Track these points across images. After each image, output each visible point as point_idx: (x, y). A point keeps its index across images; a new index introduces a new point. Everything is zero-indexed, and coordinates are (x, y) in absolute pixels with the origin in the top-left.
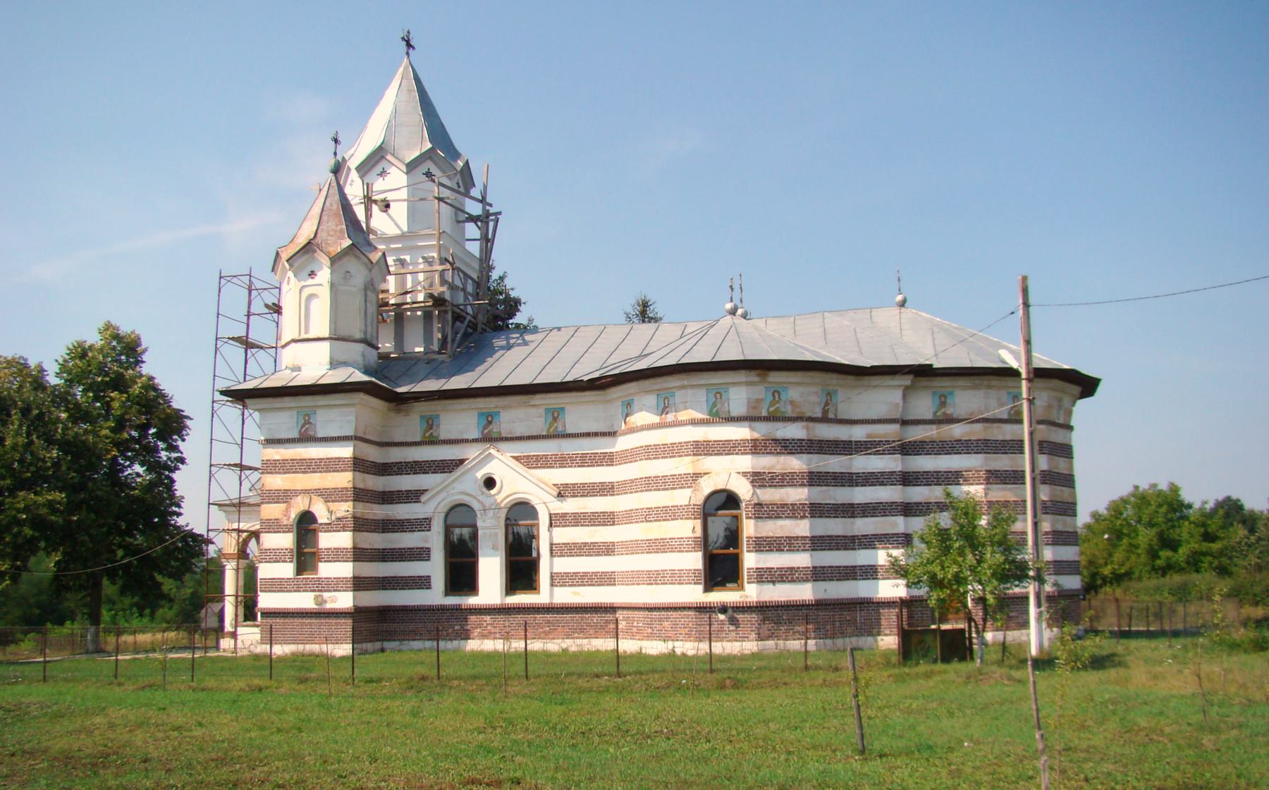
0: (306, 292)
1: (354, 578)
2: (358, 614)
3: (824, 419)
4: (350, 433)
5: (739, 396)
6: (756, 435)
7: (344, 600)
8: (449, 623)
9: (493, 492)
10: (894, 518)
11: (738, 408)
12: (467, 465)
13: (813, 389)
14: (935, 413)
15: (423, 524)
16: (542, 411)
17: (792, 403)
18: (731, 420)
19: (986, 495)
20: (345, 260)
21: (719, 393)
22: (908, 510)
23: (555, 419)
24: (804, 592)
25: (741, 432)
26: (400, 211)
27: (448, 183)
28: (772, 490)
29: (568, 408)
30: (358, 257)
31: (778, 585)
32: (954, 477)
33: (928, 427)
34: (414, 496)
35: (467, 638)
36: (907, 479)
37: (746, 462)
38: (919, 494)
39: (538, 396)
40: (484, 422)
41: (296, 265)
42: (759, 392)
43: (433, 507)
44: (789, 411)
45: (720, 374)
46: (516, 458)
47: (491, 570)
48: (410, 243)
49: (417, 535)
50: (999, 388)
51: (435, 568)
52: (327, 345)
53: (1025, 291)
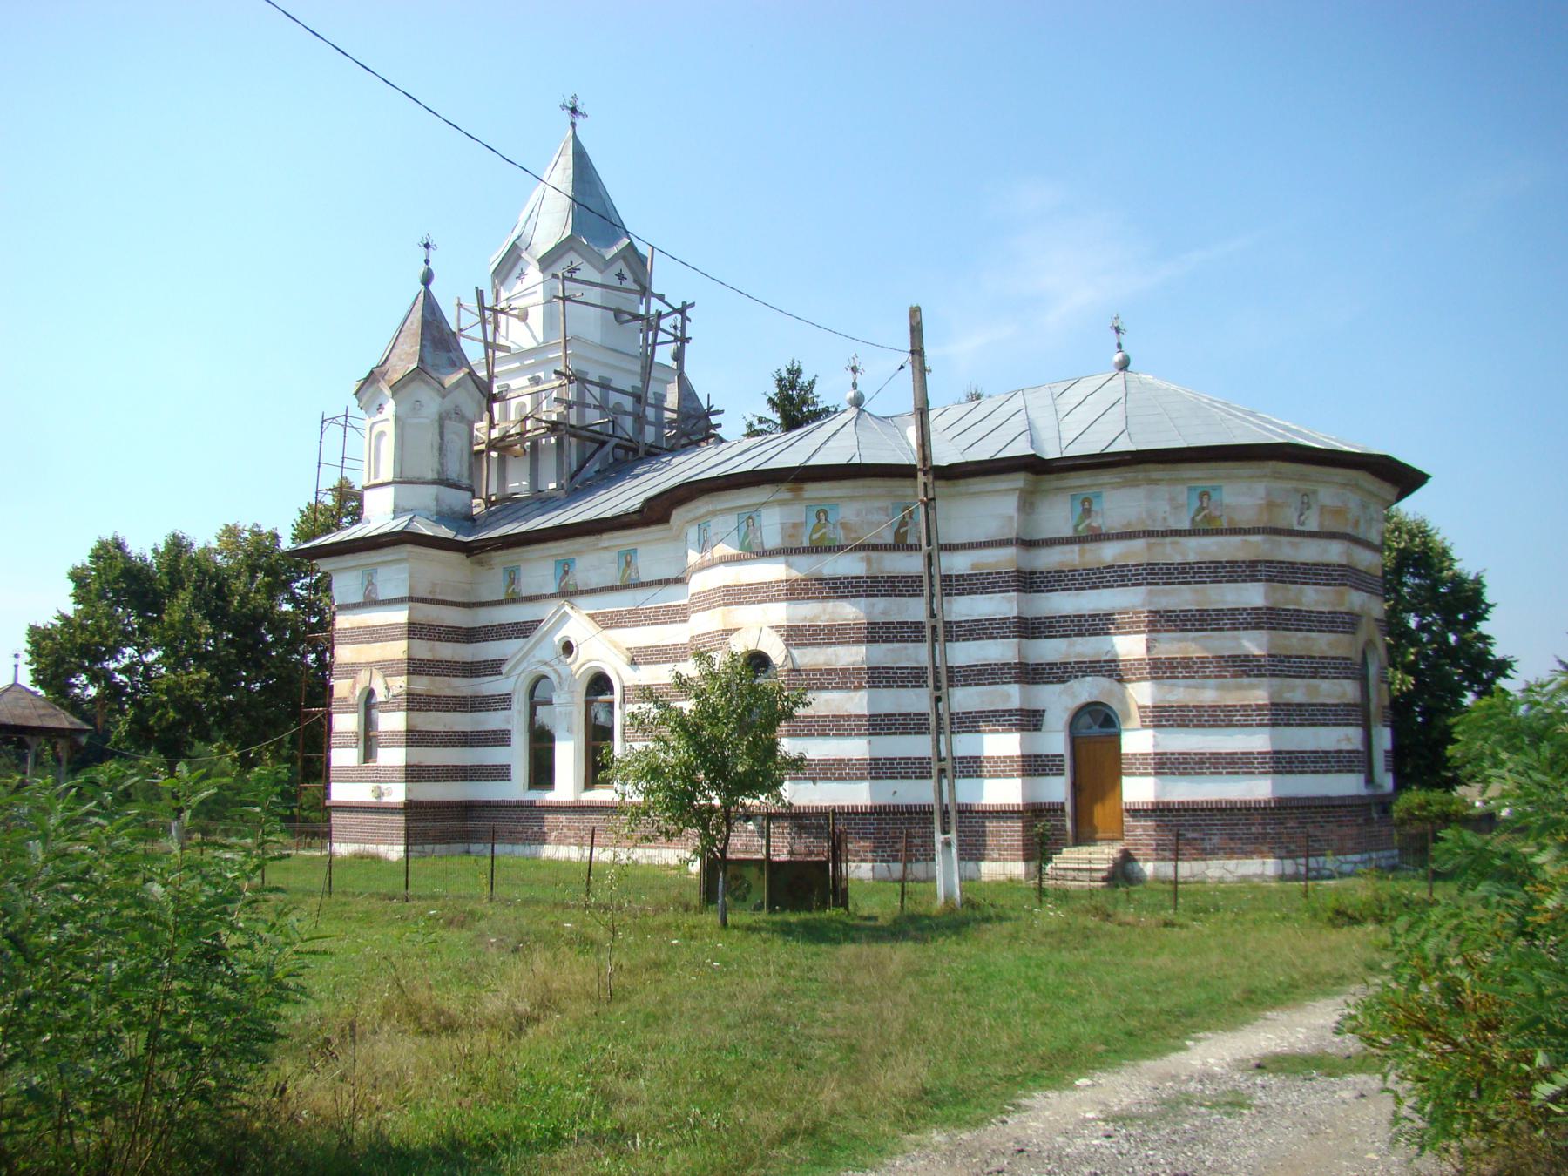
0: (377, 428)
1: (407, 766)
2: (411, 809)
3: (900, 544)
4: (405, 593)
5: (772, 523)
6: (795, 574)
7: (397, 793)
8: (524, 822)
9: (569, 660)
10: (1005, 687)
11: (772, 539)
12: (544, 628)
13: (877, 504)
16: (614, 554)
17: (844, 525)
18: (764, 554)
19: (1148, 649)
20: (413, 386)
21: (749, 518)
22: (1030, 674)
23: (628, 564)
24: (1259, 789)
25: (774, 571)
26: (536, 317)
27: (596, 277)
28: (815, 650)
29: (641, 550)
30: (428, 383)
31: (820, 784)
32: (1101, 624)
33: (1067, 548)
34: (493, 668)
36: (1029, 628)
37: (780, 612)
38: (1050, 650)
39: (605, 536)
42: (797, 513)
43: (512, 683)
44: (840, 537)
45: (744, 492)
46: (592, 616)
47: (568, 756)
48: (541, 357)
50: (1173, 482)
51: (516, 756)
52: (390, 490)
53: (916, 331)
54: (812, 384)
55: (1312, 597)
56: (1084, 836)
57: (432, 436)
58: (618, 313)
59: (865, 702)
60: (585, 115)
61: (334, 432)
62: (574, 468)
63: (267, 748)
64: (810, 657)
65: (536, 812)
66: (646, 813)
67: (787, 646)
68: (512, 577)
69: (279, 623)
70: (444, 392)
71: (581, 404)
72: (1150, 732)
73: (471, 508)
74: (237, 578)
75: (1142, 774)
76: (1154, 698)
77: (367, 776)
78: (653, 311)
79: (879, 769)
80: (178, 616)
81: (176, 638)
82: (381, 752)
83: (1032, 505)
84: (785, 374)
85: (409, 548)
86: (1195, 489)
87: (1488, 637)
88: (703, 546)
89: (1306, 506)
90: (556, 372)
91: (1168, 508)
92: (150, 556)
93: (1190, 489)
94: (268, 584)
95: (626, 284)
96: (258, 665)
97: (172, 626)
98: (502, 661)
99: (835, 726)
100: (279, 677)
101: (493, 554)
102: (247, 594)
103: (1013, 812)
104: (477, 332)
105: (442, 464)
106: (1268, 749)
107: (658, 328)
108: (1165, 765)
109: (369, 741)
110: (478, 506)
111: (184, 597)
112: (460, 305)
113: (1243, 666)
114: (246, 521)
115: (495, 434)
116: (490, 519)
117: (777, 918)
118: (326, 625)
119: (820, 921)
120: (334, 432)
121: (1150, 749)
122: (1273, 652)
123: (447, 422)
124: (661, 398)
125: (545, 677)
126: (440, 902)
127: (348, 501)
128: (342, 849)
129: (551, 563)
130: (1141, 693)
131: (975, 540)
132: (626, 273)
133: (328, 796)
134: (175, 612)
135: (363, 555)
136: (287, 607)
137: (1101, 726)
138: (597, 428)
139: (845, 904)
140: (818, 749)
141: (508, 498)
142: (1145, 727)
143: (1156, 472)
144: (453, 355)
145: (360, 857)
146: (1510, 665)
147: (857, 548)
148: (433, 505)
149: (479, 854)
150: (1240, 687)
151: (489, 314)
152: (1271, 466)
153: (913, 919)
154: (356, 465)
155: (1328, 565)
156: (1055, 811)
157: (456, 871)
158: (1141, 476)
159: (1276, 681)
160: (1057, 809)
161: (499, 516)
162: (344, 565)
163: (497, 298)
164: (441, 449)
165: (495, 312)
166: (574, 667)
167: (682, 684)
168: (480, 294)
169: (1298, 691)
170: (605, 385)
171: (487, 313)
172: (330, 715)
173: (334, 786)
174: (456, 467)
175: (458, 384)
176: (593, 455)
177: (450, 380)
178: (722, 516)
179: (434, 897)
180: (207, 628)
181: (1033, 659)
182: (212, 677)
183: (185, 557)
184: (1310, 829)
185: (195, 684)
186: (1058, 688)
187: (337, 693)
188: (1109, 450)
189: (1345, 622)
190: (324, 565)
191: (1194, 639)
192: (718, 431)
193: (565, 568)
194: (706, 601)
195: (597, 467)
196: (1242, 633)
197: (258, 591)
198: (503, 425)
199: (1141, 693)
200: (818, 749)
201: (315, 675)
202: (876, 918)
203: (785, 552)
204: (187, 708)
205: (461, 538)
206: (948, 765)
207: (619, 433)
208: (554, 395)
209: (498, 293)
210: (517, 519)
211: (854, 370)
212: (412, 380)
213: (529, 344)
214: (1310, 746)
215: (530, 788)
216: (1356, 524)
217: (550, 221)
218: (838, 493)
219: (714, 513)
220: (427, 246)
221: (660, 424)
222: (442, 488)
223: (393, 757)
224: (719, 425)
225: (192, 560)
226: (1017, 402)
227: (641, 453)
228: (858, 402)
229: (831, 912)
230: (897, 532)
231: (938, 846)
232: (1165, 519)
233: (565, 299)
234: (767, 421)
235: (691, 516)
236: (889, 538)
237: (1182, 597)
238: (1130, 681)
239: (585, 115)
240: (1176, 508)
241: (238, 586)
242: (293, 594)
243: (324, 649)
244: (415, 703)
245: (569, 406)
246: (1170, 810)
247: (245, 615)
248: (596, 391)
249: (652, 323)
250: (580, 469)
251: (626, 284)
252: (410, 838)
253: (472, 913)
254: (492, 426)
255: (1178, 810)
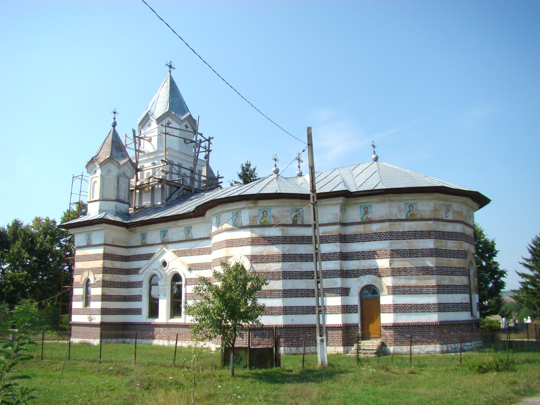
0: (94, 180)
1: (102, 309)
2: (103, 325)
3: (295, 224)
6: (254, 235)
7: (97, 319)
8: (147, 330)
9: (165, 268)
10: (335, 279)
11: (246, 222)
12: (156, 256)
14: (362, 218)
15: (139, 284)
16: (183, 228)
17: (273, 217)
18: (242, 228)
19: (390, 264)
20: (109, 164)
21: (237, 214)
22: (345, 274)
23: (188, 232)
24: (433, 318)
25: (246, 234)
26: (155, 140)
27: (178, 126)
28: (262, 264)
29: (194, 227)
30: (113, 163)
32: (371, 255)
33: (359, 226)
34: (136, 271)
35: (154, 338)
36: (344, 256)
37: (248, 250)
38: (352, 265)
39: (180, 221)
40: (162, 235)
41: (89, 169)
42: (255, 212)
43: (143, 277)
45: (235, 204)
46: (174, 252)
47: (164, 306)
48: (156, 155)
49: (135, 289)
51: (144, 305)
52: (98, 203)
53: (310, 136)
54: (254, 169)
55: (451, 245)
56: (366, 336)
57: (114, 183)
58: (185, 140)
59: (281, 285)
60: (174, 68)
61: (77, 181)
62: (168, 196)
63: (49, 301)
64: (260, 267)
65: (151, 327)
66: (201, 329)
67: (251, 263)
68: (144, 237)
69: (54, 255)
70: (119, 166)
71: (171, 173)
72: (391, 296)
73: (129, 211)
74: (39, 236)
75: (388, 312)
76: (392, 283)
77: (86, 312)
78: (198, 139)
79: (442, 308)
80: (16, 250)
81: (15, 259)
82: (91, 303)
83: (345, 209)
84: (244, 166)
85: (104, 225)
86: (407, 203)
87: (496, 263)
88: (218, 225)
89: (448, 211)
90: (162, 161)
91: (397, 211)
92: (6, 228)
93: (405, 204)
94: (51, 240)
95: (188, 129)
96: (46, 270)
97: (13, 254)
98: (139, 269)
99: (271, 294)
100: (54, 274)
101: (137, 228)
102: (43, 243)
103: (339, 327)
104: (132, 146)
105: (118, 194)
106: (436, 302)
107: (200, 146)
108: (397, 309)
109: (87, 299)
110: (131, 211)
111: (19, 243)
112: (126, 136)
113: (426, 271)
114: (43, 216)
115: (138, 183)
116: (136, 215)
117: (253, 371)
118: (72, 255)
119: (271, 372)
120: (77, 181)
121: (391, 303)
122: (437, 265)
123: (120, 178)
124: (200, 172)
125: (155, 275)
126: (114, 363)
127: (82, 207)
128: (75, 340)
129: (159, 231)
130: (388, 281)
131: (323, 223)
132: (188, 125)
133: (71, 320)
134: (14, 249)
135: (88, 227)
136: (58, 248)
137: (372, 294)
138: (177, 182)
139: (279, 366)
140: (269, 302)
141: (143, 207)
142: (389, 294)
143: (393, 197)
144: (123, 153)
145: (82, 344)
146: (505, 273)
147: (279, 226)
148: (114, 209)
149: (129, 343)
150: (425, 279)
151: (137, 139)
152: (436, 195)
153: (309, 371)
154: (85, 194)
155: (456, 233)
156: (354, 327)
157: (121, 350)
158: (387, 198)
159: (439, 276)
160: (356, 326)
161: (139, 214)
162: (79, 231)
163: (140, 133)
164: (118, 188)
165: (140, 138)
166: (167, 271)
167: (217, 275)
168: (134, 131)
169: (446, 280)
170: (180, 166)
171: (137, 139)
172: (72, 289)
173: (73, 316)
174: (123, 195)
175: (125, 164)
176: (174, 192)
177: (122, 162)
178: (226, 214)
179: (111, 362)
180: (27, 255)
181: (345, 268)
182: (28, 274)
183: (20, 228)
184: (452, 333)
185: (21, 276)
186: (355, 279)
187: (75, 280)
188: (376, 188)
189: (462, 254)
190: (71, 231)
191: (407, 261)
192: (220, 184)
193: (164, 233)
194: (219, 246)
195: (176, 196)
196: (426, 258)
197: (47, 242)
198: (141, 180)
199: (388, 281)
200: (269, 302)
201: (68, 274)
202: (292, 371)
203: (251, 227)
204: (16, 284)
205: (124, 221)
206: (322, 309)
207: (185, 184)
208: (161, 169)
209: (141, 131)
210: (147, 215)
211: (275, 160)
212: (107, 162)
213: (152, 150)
214: (451, 301)
215: (149, 318)
216: (465, 217)
217: (160, 105)
218: (271, 204)
219: (222, 212)
220: (115, 113)
221: (200, 181)
222: (118, 203)
223: (96, 305)
224: (222, 182)
225: (22, 230)
226: (337, 172)
227: (193, 191)
228: (277, 172)
229: (275, 369)
230: (293, 219)
231: (318, 342)
232: (396, 215)
233: (166, 134)
234: (238, 183)
235: (214, 213)
236: (290, 222)
237: (403, 245)
238: (383, 277)
239: (174, 68)
240: (400, 211)
241: (40, 239)
242: (60, 244)
243: (71, 265)
244: (105, 284)
245: (167, 173)
246: (399, 326)
247: (41, 250)
248: (177, 168)
249: (198, 144)
250: (170, 197)
251: (188, 129)
252: (102, 337)
253: (127, 369)
254: (137, 180)
255: (402, 326)
